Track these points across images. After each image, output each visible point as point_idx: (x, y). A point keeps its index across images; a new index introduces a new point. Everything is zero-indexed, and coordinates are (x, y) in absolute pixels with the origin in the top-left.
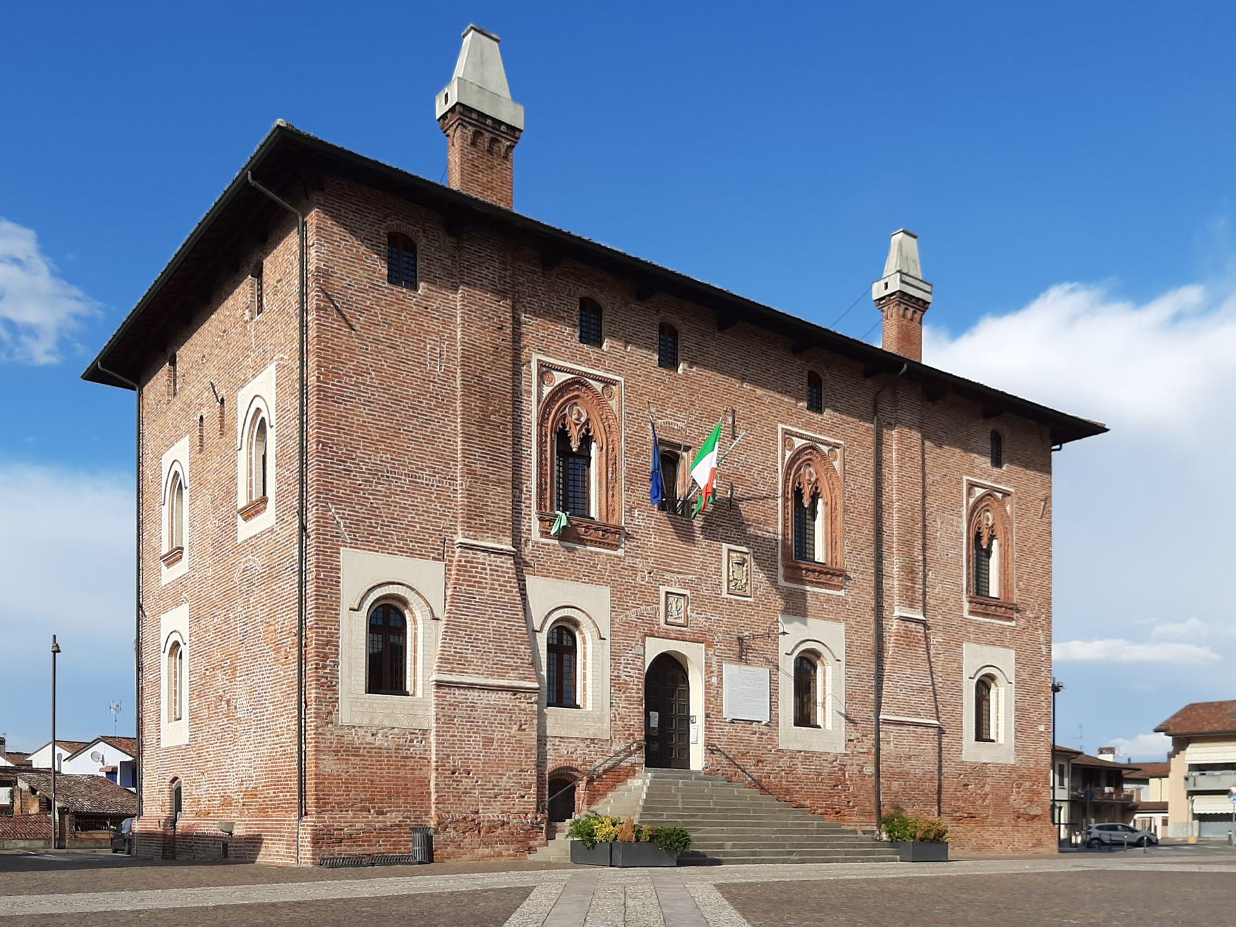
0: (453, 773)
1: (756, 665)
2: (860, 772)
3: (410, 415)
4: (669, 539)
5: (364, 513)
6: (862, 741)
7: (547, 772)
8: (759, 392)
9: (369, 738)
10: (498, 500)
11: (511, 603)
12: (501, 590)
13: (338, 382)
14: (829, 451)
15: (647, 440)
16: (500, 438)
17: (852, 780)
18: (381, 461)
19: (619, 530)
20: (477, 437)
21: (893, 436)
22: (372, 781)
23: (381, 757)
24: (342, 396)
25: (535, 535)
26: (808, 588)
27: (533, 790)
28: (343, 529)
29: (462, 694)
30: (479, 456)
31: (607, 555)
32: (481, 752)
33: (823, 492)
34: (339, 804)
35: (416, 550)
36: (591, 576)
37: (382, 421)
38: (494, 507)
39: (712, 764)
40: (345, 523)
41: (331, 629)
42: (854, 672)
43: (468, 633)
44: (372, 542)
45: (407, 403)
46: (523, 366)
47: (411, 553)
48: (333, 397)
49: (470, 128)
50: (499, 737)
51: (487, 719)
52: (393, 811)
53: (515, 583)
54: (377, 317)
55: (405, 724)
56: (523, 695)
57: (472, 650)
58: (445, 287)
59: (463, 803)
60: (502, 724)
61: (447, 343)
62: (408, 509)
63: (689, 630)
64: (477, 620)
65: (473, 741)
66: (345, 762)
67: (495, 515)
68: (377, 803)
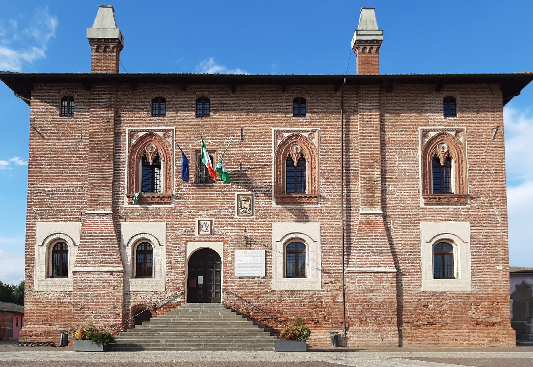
0: (81, 309)
1: (257, 249)
2: (333, 300)
3: (67, 166)
4: (202, 195)
5: (46, 208)
6: (335, 283)
7: (130, 307)
8: (259, 116)
9: (46, 296)
10: (106, 193)
11: (110, 235)
12: (105, 230)
13: (37, 159)
14: (309, 135)
15: (189, 152)
16: (107, 167)
17: (327, 305)
18: (54, 186)
19: (171, 196)
20: (96, 168)
21: (357, 120)
22: (47, 313)
23: (51, 303)
24: (39, 164)
25: (126, 205)
26: (304, 206)
27: (121, 315)
28: (37, 215)
29: (85, 276)
30: (96, 176)
31: (165, 208)
32: (94, 300)
33: (307, 156)
34: (33, 322)
35: (68, 219)
36: (456, 217)
37: (55, 170)
38: (103, 196)
39: (227, 300)
40: (38, 212)
41: (31, 254)
42: (328, 246)
43: (89, 250)
44: (49, 218)
45: (66, 161)
46: (122, 134)
47: (66, 220)
48: (35, 166)
49: (95, 46)
50: (103, 293)
51: (97, 285)
52: (55, 325)
53: (112, 226)
54: (54, 131)
55: (62, 290)
56: (115, 274)
57: (90, 257)
58: (84, 111)
59: (86, 321)
60: (104, 287)
61: (85, 133)
62: (65, 203)
63: (213, 236)
64: (93, 244)
65: (90, 295)
66: (36, 305)
67: (103, 199)
68: (49, 321)
